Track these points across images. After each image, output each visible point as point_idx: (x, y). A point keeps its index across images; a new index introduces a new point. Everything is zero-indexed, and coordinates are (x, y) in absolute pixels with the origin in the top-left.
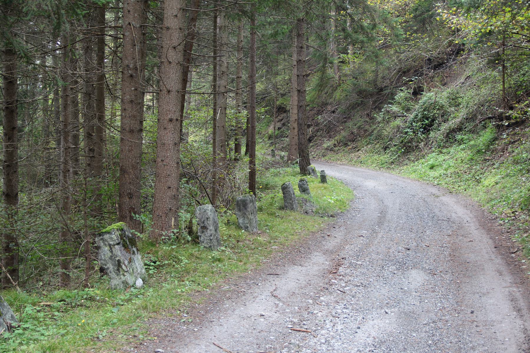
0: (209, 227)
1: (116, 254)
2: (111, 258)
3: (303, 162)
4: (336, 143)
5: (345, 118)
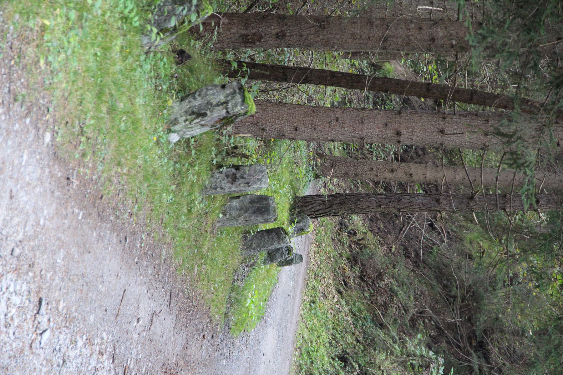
0: (234, 185)
1: (215, 111)
2: (209, 103)
3: (320, 204)
4: (359, 236)
5: (417, 255)
